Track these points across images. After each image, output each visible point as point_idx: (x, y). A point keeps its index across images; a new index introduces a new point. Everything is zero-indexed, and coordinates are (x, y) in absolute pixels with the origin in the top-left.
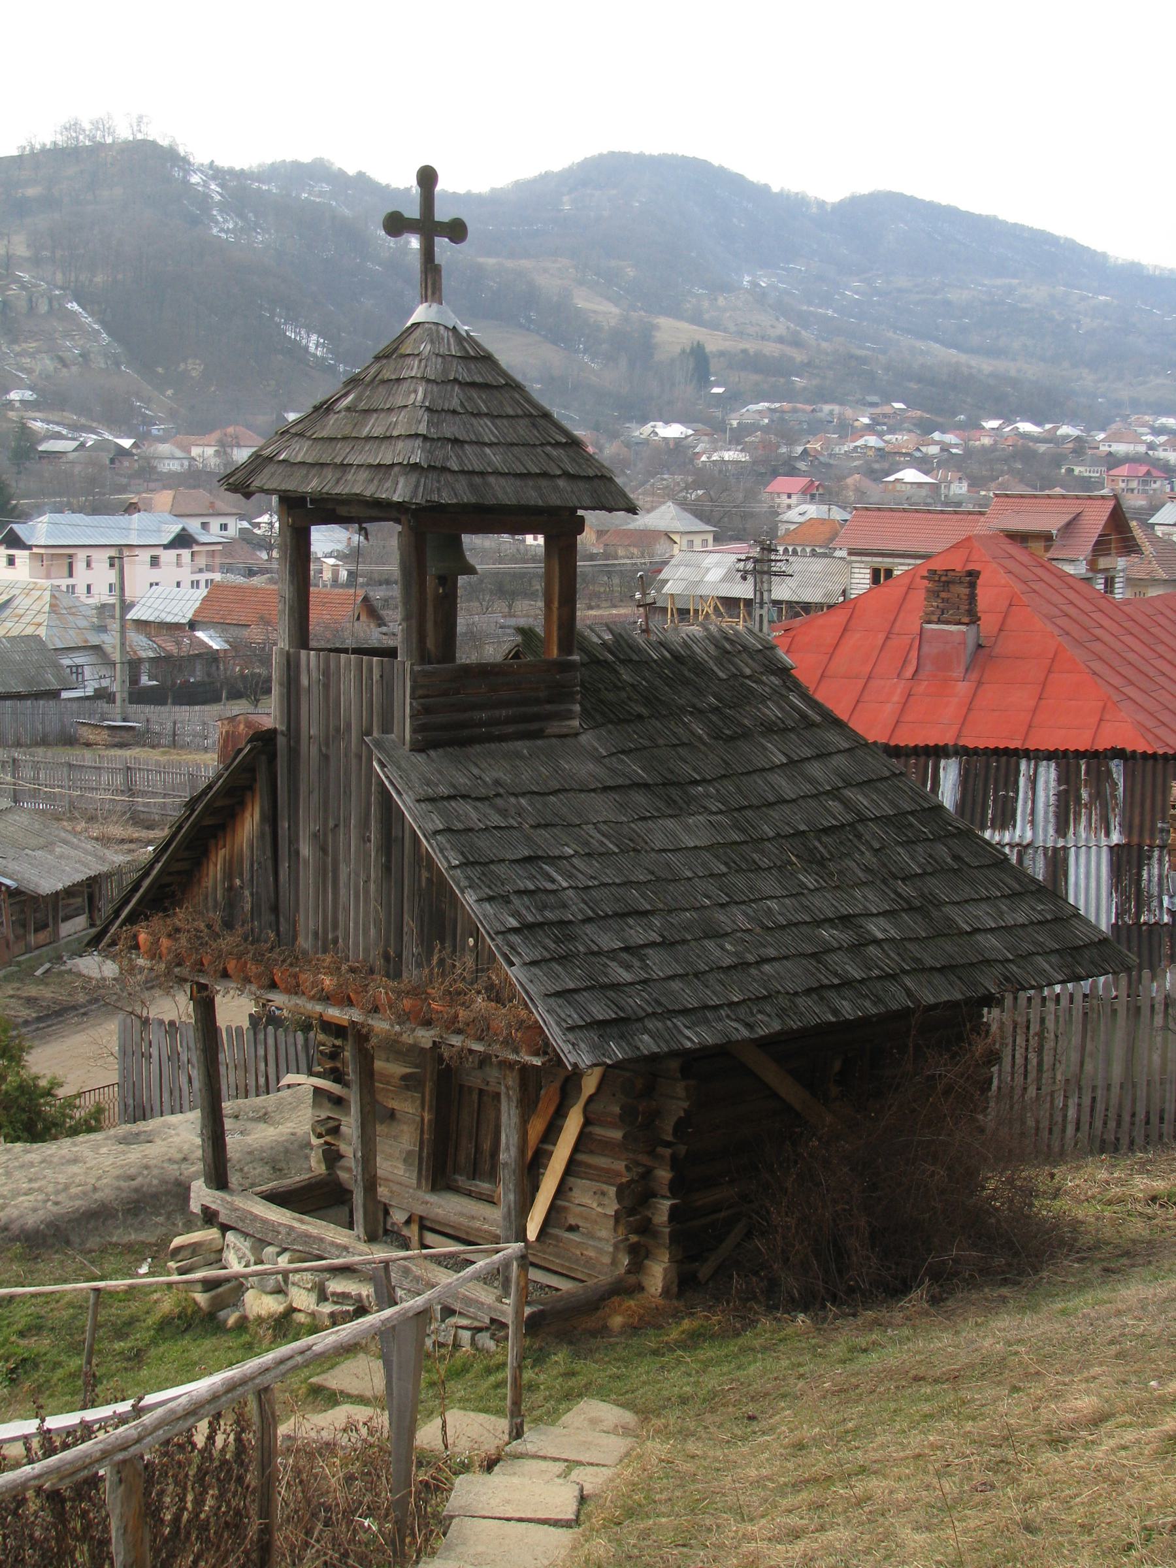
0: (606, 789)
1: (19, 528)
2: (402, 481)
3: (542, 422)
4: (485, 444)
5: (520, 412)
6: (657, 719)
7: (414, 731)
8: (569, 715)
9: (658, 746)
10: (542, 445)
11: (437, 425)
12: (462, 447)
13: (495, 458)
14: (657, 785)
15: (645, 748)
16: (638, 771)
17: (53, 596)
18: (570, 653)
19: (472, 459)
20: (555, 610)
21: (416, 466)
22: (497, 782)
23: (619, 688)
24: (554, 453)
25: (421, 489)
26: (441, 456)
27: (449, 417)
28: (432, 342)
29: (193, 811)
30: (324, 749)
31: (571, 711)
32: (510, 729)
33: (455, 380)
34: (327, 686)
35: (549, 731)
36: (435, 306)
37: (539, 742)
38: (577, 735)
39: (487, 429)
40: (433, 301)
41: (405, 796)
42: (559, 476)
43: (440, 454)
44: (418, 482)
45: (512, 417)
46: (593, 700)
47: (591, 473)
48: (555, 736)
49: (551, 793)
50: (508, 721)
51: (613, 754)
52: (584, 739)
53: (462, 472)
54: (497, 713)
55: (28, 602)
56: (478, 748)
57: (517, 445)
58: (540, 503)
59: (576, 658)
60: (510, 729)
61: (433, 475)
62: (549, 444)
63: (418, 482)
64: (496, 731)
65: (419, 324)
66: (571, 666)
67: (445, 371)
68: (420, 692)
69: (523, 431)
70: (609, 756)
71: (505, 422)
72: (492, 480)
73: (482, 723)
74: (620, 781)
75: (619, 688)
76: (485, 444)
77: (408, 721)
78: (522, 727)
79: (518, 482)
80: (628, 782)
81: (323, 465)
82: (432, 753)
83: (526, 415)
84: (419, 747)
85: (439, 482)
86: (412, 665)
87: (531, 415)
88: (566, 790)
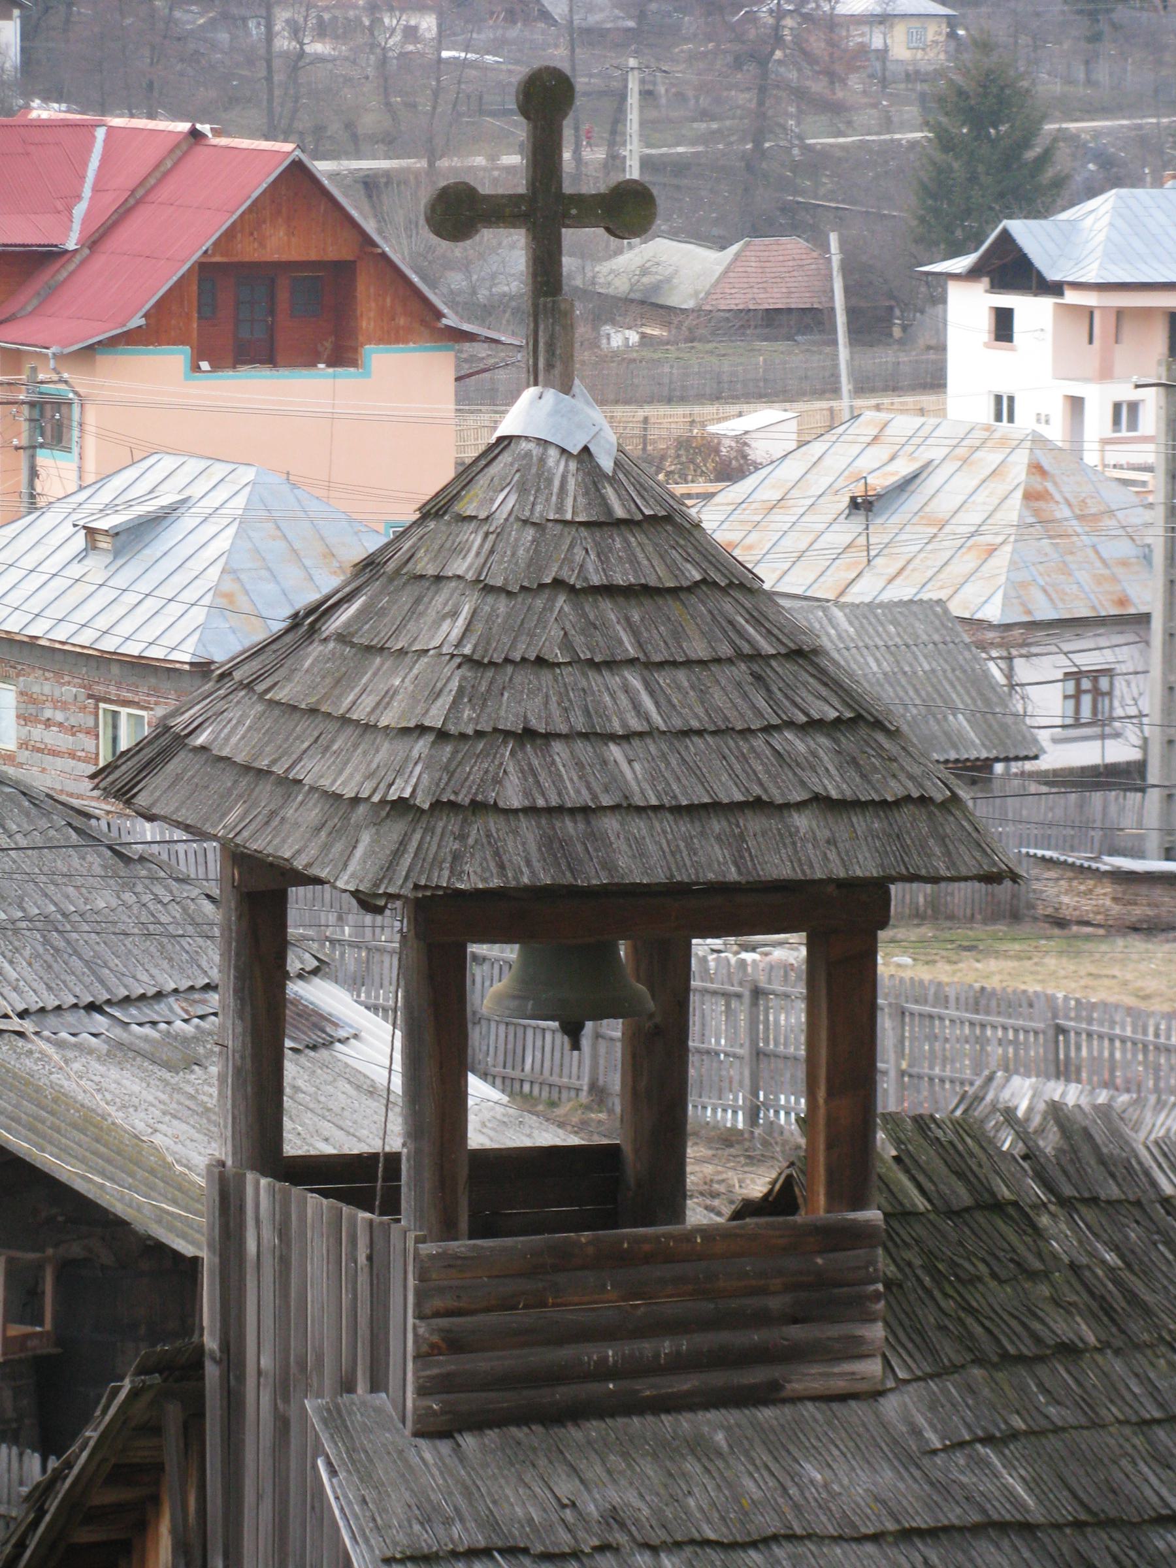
0: (907, 1535)
1: (1026, 232)
2: (366, 838)
3: (786, 669)
4: (613, 737)
5: (725, 650)
6: (1117, 1352)
7: (421, 1391)
8: (855, 1350)
9: (1097, 1425)
10: (768, 729)
11: (482, 701)
12: (548, 745)
13: (631, 770)
14: (1058, 1526)
15: (1057, 1430)
16: (1011, 1484)
17: (1037, 469)
18: (859, 1203)
19: (567, 776)
20: (821, 1101)
21: (402, 806)
22: (614, 1517)
23: (1033, 1275)
24: (799, 745)
25: (407, 859)
26: (476, 776)
27: (523, 678)
28: (522, 489)
29: (41, 1513)
30: (280, 1405)
31: (859, 1340)
32: (686, 1383)
33: (558, 583)
34: (284, 1262)
35: (796, 1387)
36: (551, 395)
37: (766, 1414)
38: (878, 1394)
39: (629, 699)
40: (548, 384)
41: (595, 1491)
42: (800, 806)
43: (475, 770)
44: (403, 844)
45: (701, 662)
46: (949, 1305)
47: (893, 790)
48: (814, 1399)
49: (754, 1544)
50: (679, 1365)
51: (962, 1444)
52: (890, 1405)
53: (531, 811)
54: (646, 1347)
55: (965, 482)
56: (594, 1428)
57: (700, 733)
58: (733, 875)
59: (873, 1215)
60: (686, 1383)
61: (448, 824)
62: (790, 724)
63: (403, 844)
64: (646, 1388)
65: (510, 438)
66: (859, 1235)
67: (536, 562)
68: (437, 1303)
69: (729, 697)
70: (945, 1449)
71: (681, 676)
72: (610, 824)
73: (604, 1372)
74: (953, 1515)
75: (1033, 1275)
76: (613, 737)
77: (410, 1366)
78: (718, 1379)
79: (685, 827)
80: (975, 1517)
81: (263, 774)
82: (469, 1441)
83: (742, 656)
84: (437, 1429)
85: (462, 837)
86: (418, 1240)
87: (757, 656)
88: (792, 1537)
